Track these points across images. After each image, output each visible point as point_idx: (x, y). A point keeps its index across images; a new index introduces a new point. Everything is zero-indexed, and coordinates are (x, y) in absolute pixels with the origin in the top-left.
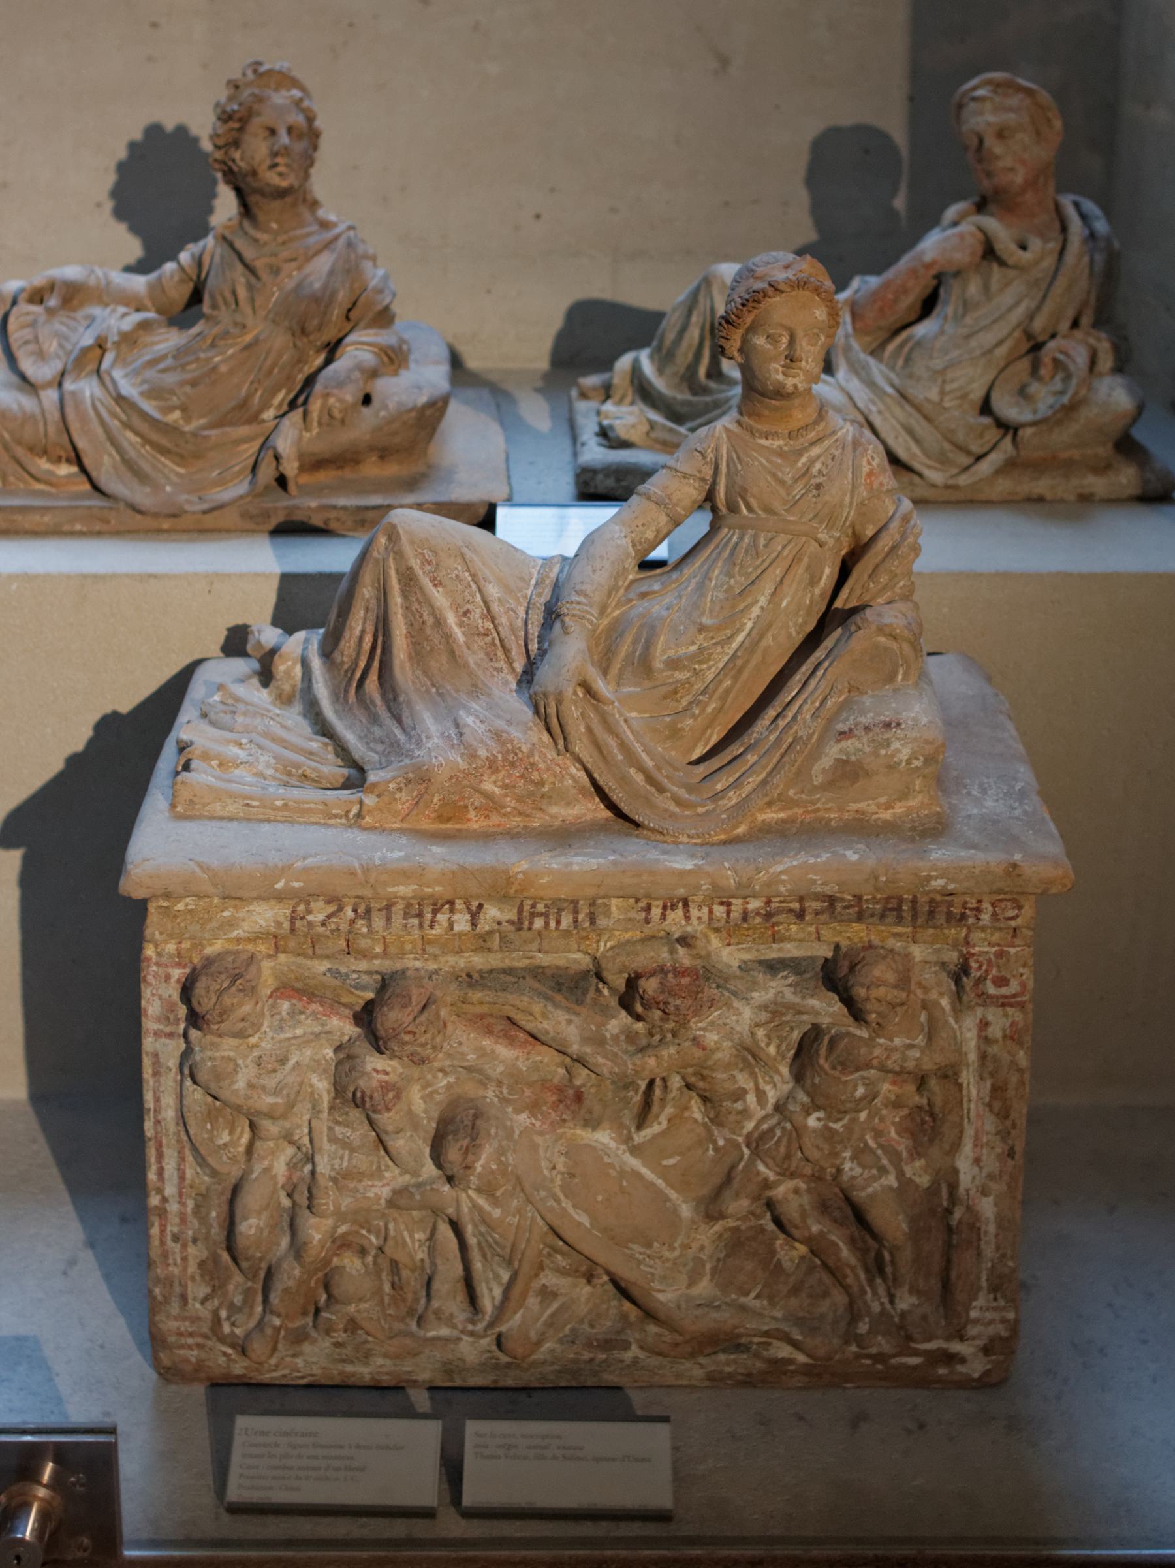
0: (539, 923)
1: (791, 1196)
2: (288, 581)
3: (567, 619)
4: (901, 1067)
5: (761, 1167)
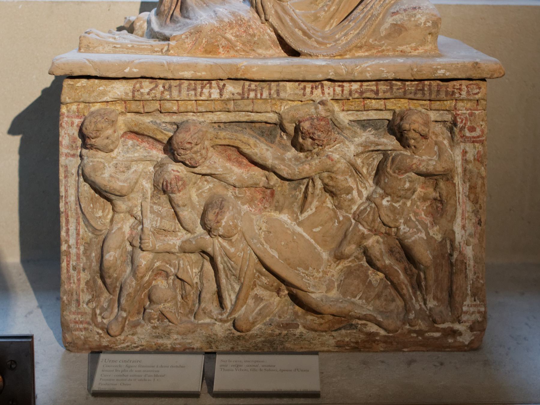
0: (252, 95)
1: (375, 244)
4: (427, 169)
5: (361, 227)
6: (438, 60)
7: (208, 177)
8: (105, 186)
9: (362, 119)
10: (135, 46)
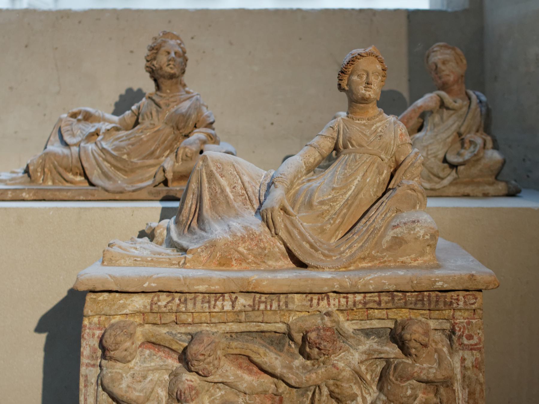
0: (262, 307)
2: (164, 209)
3: (276, 183)
4: (427, 377)
6: (437, 272)
7: (220, 385)
8: (122, 396)
9: (365, 328)
10: (154, 259)
